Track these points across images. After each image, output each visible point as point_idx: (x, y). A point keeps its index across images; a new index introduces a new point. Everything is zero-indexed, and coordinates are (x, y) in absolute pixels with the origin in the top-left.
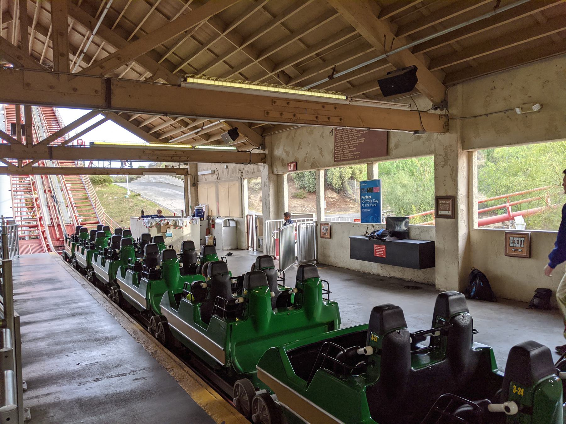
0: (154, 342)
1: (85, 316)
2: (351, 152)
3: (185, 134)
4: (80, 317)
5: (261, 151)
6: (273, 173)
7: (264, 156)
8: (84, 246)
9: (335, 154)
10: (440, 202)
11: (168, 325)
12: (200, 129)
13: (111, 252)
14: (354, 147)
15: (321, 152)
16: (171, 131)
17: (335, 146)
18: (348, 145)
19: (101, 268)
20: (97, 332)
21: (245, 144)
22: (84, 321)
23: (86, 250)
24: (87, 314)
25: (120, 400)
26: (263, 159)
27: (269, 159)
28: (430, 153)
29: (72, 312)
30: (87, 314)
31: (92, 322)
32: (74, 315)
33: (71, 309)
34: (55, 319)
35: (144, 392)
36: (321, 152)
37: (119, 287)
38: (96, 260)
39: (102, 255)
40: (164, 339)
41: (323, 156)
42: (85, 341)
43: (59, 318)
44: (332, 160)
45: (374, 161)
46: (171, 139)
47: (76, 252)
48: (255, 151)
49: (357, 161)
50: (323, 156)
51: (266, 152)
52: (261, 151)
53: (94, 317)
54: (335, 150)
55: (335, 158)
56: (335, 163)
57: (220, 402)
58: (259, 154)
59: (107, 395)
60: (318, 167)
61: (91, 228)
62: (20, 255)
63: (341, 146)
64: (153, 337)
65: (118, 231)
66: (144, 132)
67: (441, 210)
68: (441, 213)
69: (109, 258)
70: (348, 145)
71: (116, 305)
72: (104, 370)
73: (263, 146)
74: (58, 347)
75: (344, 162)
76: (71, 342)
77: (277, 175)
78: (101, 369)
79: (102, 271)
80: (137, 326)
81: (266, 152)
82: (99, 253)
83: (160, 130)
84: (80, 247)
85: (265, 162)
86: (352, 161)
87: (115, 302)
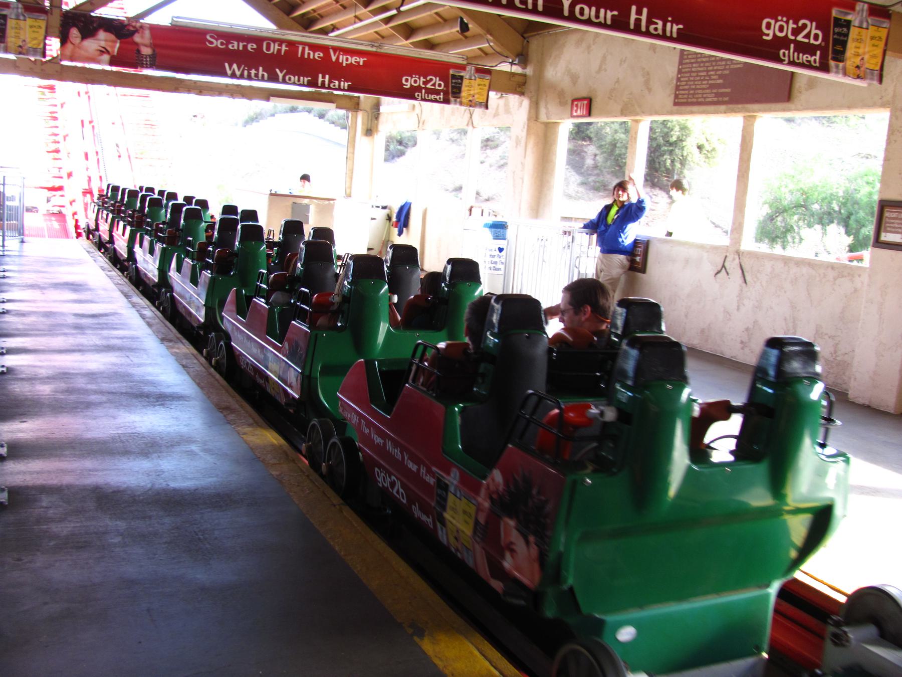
0: (250, 416)
1: (128, 354)
2: (712, 87)
3: (361, 20)
4: (117, 354)
5: (516, 69)
6: (537, 118)
7: (521, 79)
8: (157, 236)
9: (677, 88)
10: (887, 214)
11: (232, 346)
12: (394, 12)
13: (214, 252)
14: (720, 77)
15: (647, 83)
16: (335, 13)
17: (680, 71)
18: (708, 71)
19: (190, 289)
20: (147, 383)
21: (486, 54)
22: (124, 360)
23: (158, 247)
24: (131, 349)
25: (172, 501)
26: (518, 85)
27: (531, 86)
28: (883, 105)
29: (104, 342)
30: (131, 349)
31: (139, 365)
32: (109, 348)
33: (107, 338)
34: (73, 351)
35: (218, 495)
36: (647, 83)
37: (228, 338)
38: (179, 270)
39: (163, 243)
40: (134, 278)
41: (650, 90)
42: (122, 393)
43: (80, 351)
44: (670, 101)
45: (760, 111)
46: (333, 31)
47: (173, 274)
48: (505, 67)
49: (723, 107)
50: (650, 90)
51: (529, 71)
52: (516, 69)
53: (144, 359)
54: (678, 79)
55: (676, 96)
56: (676, 108)
57: (274, 448)
58: (513, 75)
59: (150, 489)
60: (637, 114)
61: (489, 284)
62: (26, 239)
63: (691, 72)
64: (199, 356)
65: (188, 200)
66: (281, 14)
67: (886, 231)
68: (886, 237)
69: (207, 266)
70: (708, 71)
71: (218, 376)
72: (151, 446)
73: (523, 58)
74: (73, 397)
75: (695, 108)
76: (96, 392)
77: (547, 125)
78: (143, 446)
79: (192, 297)
80: (186, 348)
81: (529, 71)
82: (188, 254)
83: (314, 11)
84: (147, 238)
85: (522, 94)
86: (712, 108)
87: (215, 368)
